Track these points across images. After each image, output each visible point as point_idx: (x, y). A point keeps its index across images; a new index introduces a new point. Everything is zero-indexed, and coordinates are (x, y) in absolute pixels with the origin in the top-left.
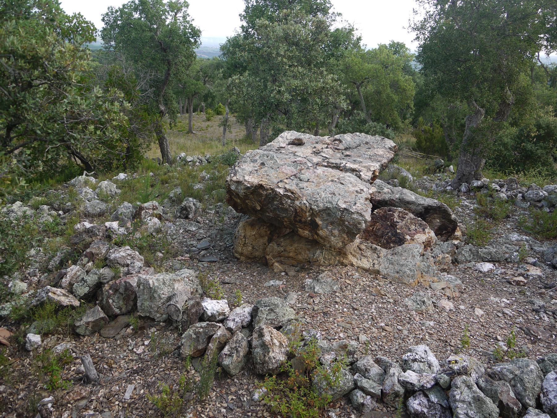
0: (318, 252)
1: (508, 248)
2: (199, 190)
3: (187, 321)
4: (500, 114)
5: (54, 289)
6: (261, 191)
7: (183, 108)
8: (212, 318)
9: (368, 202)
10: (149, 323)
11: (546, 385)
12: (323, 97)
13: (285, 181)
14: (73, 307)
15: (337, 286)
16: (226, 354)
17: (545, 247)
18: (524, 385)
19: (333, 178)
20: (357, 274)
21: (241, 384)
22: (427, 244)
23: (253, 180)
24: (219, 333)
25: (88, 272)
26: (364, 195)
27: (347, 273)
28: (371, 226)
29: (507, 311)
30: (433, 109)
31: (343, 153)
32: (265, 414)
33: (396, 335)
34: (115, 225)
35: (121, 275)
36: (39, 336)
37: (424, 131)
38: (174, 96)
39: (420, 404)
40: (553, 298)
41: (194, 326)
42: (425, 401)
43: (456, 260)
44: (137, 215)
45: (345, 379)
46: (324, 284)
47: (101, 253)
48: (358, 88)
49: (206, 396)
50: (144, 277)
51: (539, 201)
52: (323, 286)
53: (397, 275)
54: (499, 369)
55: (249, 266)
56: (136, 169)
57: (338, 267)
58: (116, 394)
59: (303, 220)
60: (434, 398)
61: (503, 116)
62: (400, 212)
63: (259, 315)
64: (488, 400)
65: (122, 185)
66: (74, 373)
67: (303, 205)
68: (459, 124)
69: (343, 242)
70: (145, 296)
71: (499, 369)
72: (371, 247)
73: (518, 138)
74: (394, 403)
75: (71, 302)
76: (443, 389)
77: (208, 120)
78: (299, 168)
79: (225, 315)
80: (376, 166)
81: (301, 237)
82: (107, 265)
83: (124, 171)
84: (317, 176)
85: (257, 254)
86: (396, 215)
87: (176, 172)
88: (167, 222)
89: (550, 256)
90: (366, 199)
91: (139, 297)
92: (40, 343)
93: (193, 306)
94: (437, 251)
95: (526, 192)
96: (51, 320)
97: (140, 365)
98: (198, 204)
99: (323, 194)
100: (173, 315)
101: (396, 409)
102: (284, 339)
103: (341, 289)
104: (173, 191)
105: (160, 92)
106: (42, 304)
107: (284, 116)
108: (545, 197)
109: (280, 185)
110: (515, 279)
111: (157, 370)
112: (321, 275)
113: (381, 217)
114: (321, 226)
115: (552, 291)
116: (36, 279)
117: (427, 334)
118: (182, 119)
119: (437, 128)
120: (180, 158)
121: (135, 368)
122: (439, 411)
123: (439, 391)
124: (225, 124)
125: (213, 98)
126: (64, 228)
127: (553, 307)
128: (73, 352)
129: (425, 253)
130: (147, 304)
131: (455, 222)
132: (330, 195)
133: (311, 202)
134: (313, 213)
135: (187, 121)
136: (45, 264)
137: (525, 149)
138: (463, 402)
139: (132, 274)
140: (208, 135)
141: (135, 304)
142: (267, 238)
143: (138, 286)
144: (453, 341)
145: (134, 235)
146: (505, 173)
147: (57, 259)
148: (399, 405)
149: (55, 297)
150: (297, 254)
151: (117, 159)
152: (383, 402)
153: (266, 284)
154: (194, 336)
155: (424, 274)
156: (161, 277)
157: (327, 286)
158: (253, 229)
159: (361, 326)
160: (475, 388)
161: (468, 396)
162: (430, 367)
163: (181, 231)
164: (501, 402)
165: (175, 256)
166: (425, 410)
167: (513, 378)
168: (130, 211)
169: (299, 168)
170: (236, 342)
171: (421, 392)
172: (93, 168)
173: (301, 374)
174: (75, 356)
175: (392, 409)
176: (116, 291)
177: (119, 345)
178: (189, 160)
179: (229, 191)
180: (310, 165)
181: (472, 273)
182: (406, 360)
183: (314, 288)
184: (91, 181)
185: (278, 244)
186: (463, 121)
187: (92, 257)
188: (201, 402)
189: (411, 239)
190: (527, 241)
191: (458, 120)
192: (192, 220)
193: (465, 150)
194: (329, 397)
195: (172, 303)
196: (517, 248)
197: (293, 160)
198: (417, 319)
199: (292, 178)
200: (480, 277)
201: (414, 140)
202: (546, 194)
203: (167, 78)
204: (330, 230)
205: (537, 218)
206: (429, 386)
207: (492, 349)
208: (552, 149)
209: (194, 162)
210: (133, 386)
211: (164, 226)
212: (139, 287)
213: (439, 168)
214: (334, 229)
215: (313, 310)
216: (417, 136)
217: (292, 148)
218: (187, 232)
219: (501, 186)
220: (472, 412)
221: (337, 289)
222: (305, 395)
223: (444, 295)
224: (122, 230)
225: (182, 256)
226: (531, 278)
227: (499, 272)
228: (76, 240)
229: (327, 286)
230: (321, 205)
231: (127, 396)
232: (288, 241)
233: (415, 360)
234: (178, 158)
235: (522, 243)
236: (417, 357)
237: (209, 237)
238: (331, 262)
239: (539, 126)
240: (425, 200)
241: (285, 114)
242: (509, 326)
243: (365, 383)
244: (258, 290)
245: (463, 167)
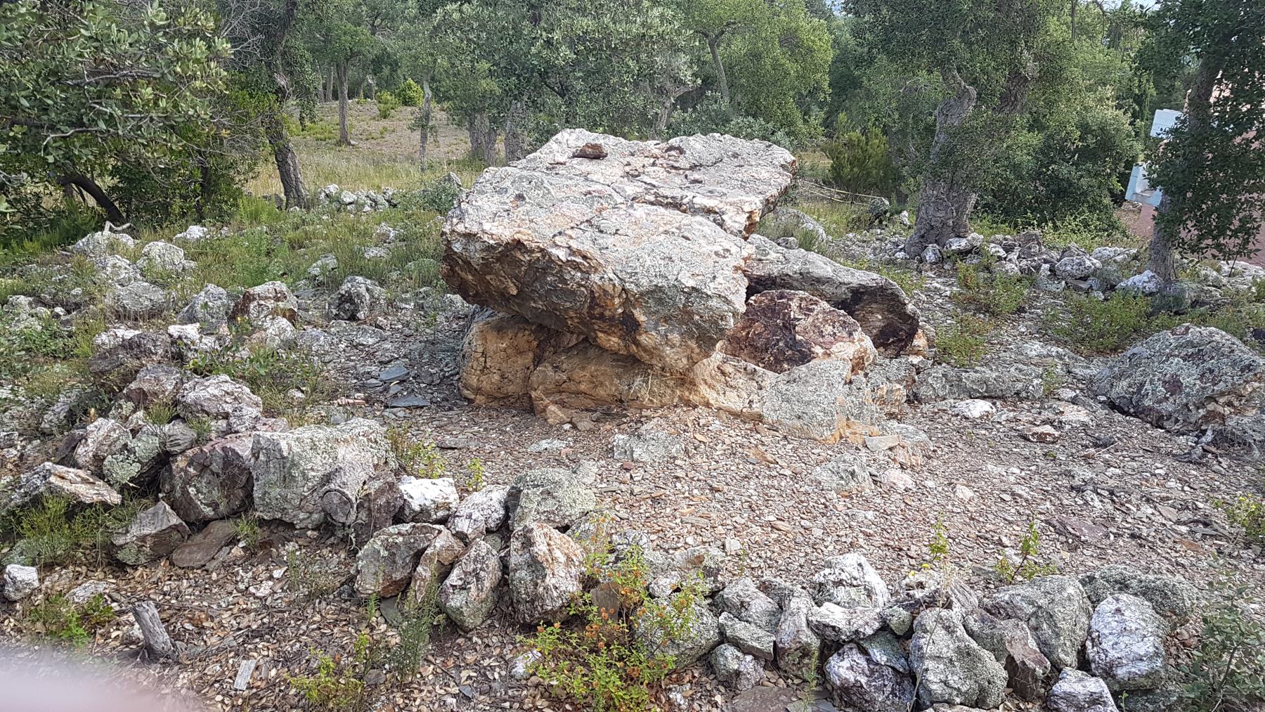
0: (638, 380)
1: (1021, 371)
2: (376, 261)
3: (367, 525)
4: (1008, 99)
5: (61, 469)
6: (519, 255)
7: (325, 87)
8: (422, 515)
9: (739, 275)
10: (281, 531)
11: (1097, 624)
12: (643, 56)
13: (569, 232)
14: (106, 506)
16: (454, 587)
17: (1096, 369)
18: (1055, 625)
19: (668, 227)
21: (488, 645)
22: (858, 364)
23: (502, 231)
24: (439, 543)
25: (134, 432)
26: (733, 261)
27: (697, 420)
28: (743, 329)
29: (1018, 490)
30: (869, 96)
32: (538, 703)
33: (800, 539)
34: (191, 330)
35: (213, 435)
36: (34, 569)
37: (850, 145)
38: (308, 55)
39: (852, 668)
40: (1109, 466)
41: (384, 533)
42: (862, 661)
43: (915, 395)
44: (239, 309)
45: (700, 626)
46: (652, 443)
47: (164, 392)
48: (711, 45)
49: (414, 675)
50: (268, 435)
51: (1084, 279)
54: (1006, 598)
55: (494, 414)
56: (227, 218)
57: (678, 411)
58: (216, 681)
59: (607, 313)
60: (879, 655)
61: (1014, 105)
62: (801, 299)
63: (522, 503)
64: (987, 655)
65: (196, 251)
66: (117, 643)
68: (922, 126)
69: (689, 358)
70: (271, 476)
71: (1006, 598)
73: (1043, 153)
74: (799, 669)
75: (103, 495)
76: (898, 637)
77: (385, 116)
78: (596, 206)
79: (449, 509)
80: (754, 203)
81: (602, 349)
82: (177, 417)
83: (199, 221)
85: (511, 389)
86: (794, 304)
87: (319, 223)
88: (309, 328)
89: (1105, 384)
90: (737, 269)
91: (257, 480)
92: (36, 584)
93: (381, 491)
94: (876, 377)
95: (1059, 260)
96: (56, 535)
97: (265, 620)
98: (378, 290)
100: (336, 513)
101: (805, 681)
102: (576, 550)
103: (686, 451)
104: (319, 262)
105: (275, 44)
106: (36, 502)
107: (559, 101)
108: (1096, 269)
110: (1036, 429)
111: (304, 627)
112: (644, 428)
115: (1108, 451)
116: (15, 452)
117: (861, 535)
118: (328, 113)
119: (876, 135)
120: (327, 195)
121: (254, 627)
122: (890, 680)
123: (889, 641)
124: (423, 124)
125: (395, 66)
126: (70, 342)
127: (1111, 482)
128: (113, 601)
130: (275, 492)
132: (662, 262)
135: (337, 118)
136: (33, 422)
137: (1057, 177)
138: (938, 658)
139: (237, 432)
140: (385, 150)
141: (249, 496)
142: (531, 355)
143: (254, 455)
144: (913, 548)
145: (237, 350)
146: (1016, 226)
147: (61, 407)
148: (811, 675)
149: (66, 485)
151: (181, 196)
152: (779, 669)
153: (533, 448)
154: (384, 553)
155: (852, 419)
156: (306, 435)
158: (502, 338)
159: (728, 522)
160: (961, 631)
161: (948, 646)
162: (869, 596)
163: (342, 346)
164: (1010, 659)
165: (332, 395)
166: (863, 680)
167: (1034, 613)
168: (223, 305)
169: (596, 206)
170: (475, 560)
171: (853, 645)
172: (124, 215)
173: (611, 616)
174: (118, 608)
175: (796, 681)
176: (204, 468)
177: (216, 582)
178: (348, 200)
179: (449, 256)
180: (619, 200)
181: (949, 420)
182: (821, 584)
183: (632, 452)
184: (125, 244)
186: (930, 119)
187: (142, 399)
188: (402, 687)
189: (825, 354)
190: (1060, 357)
191: (921, 116)
192: (365, 323)
193: (935, 174)
194: (671, 655)
195: (332, 486)
196: (1040, 370)
197: (584, 190)
198: (840, 506)
200: (964, 428)
201: (827, 163)
202: (1099, 265)
203: (290, 13)
205: (1079, 310)
206: (869, 632)
207: (992, 562)
208: (1110, 175)
209: (359, 205)
210: (252, 664)
211: (302, 336)
212: (257, 458)
213: (879, 218)
214: (672, 331)
215: (632, 493)
216: (832, 153)
218: (356, 347)
219: (1009, 249)
220: (956, 678)
222: (621, 659)
223: (894, 460)
224: (209, 342)
225: (348, 397)
226: (1068, 427)
227: (1004, 417)
228: (104, 365)
230: (644, 282)
231: (241, 683)
232: (576, 360)
233: (839, 583)
234: (323, 195)
235: (1049, 360)
236: (843, 576)
237: (405, 356)
239: (1085, 129)
241: (563, 96)
242: (1025, 518)
243: (740, 630)
244: (517, 459)
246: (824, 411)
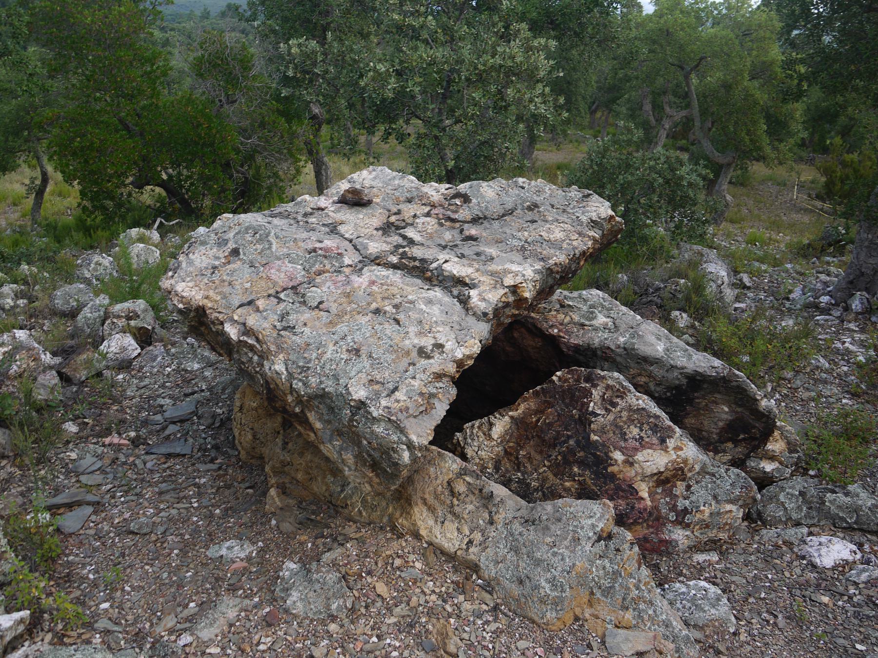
15: (341, 601)
20: (418, 565)
52: (312, 594)
53: (516, 590)
84: (348, 295)
90: (439, 376)
99: (331, 347)
113: (563, 391)
129: (616, 530)
131: (768, 417)
132: (345, 356)
157: (319, 596)
199: (282, 296)
214: (346, 449)
221: (339, 608)
229: (319, 596)
230: (313, 381)
238: (375, 515)
245: (862, 257)
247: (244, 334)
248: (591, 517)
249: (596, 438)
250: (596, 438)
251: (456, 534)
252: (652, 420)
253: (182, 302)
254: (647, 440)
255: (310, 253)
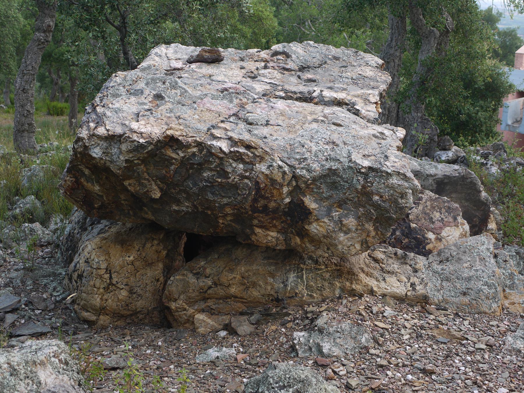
6: (170, 153)
15: (366, 335)
23: (150, 128)
27: (368, 308)
31: (299, 77)
52: (338, 340)
53: (466, 300)
57: (345, 301)
67: (276, 171)
72: (396, 254)
78: (236, 101)
85: (140, 304)
109: (217, 133)
114: (316, 212)
132: (327, 147)
133: (293, 162)
134: (297, 186)
142: (161, 265)
150: (247, 288)
155: (508, 291)
158: (127, 251)
185: (195, 274)
204: (336, 218)
214: (346, 216)
217: (200, 68)
219: (485, 156)
221: (367, 341)
230: (315, 166)
232: (220, 264)
240: (436, 168)
246: (486, 284)
247: (232, 146)
248: (483, 244)
249: (414, 225)
250: (414, 225)
251: (399, 283)
252: (446, 204)
253: (142, 137)
254: (446, 220)
255: (222, 92)
